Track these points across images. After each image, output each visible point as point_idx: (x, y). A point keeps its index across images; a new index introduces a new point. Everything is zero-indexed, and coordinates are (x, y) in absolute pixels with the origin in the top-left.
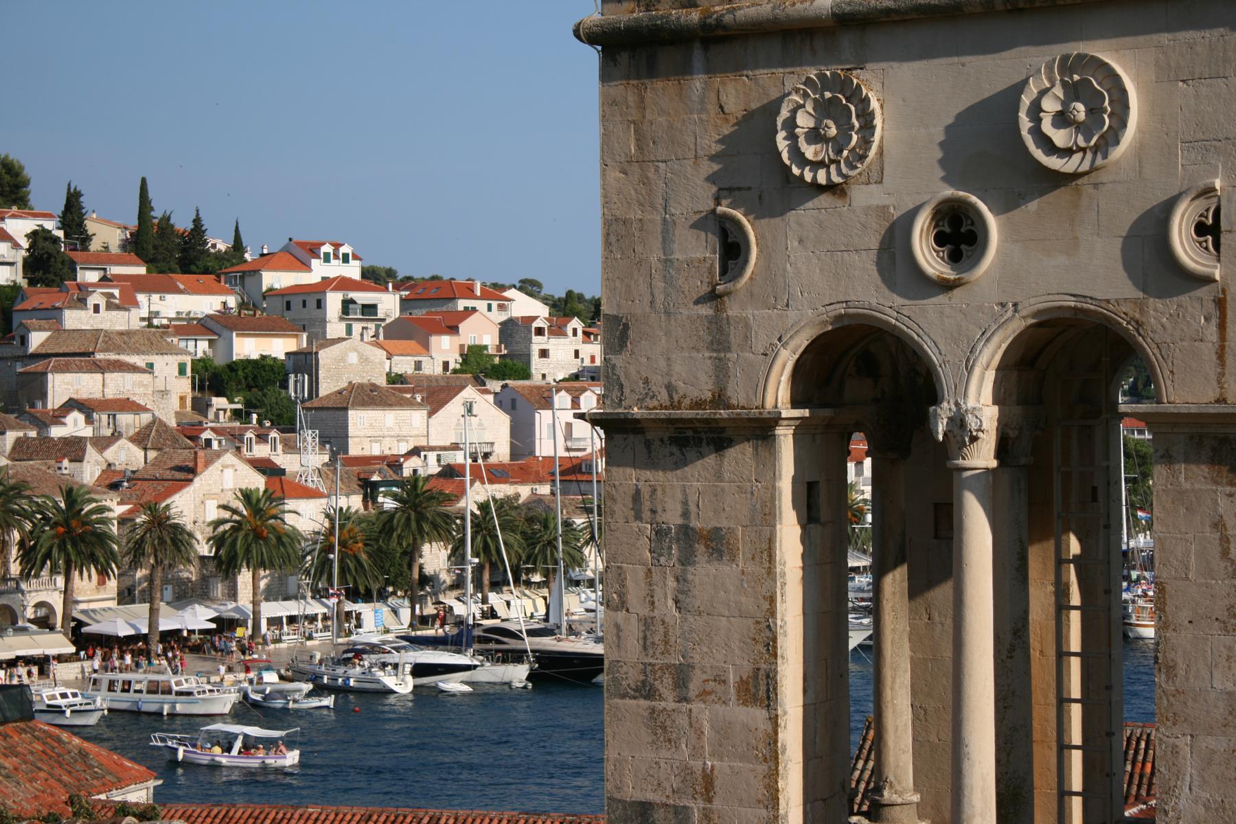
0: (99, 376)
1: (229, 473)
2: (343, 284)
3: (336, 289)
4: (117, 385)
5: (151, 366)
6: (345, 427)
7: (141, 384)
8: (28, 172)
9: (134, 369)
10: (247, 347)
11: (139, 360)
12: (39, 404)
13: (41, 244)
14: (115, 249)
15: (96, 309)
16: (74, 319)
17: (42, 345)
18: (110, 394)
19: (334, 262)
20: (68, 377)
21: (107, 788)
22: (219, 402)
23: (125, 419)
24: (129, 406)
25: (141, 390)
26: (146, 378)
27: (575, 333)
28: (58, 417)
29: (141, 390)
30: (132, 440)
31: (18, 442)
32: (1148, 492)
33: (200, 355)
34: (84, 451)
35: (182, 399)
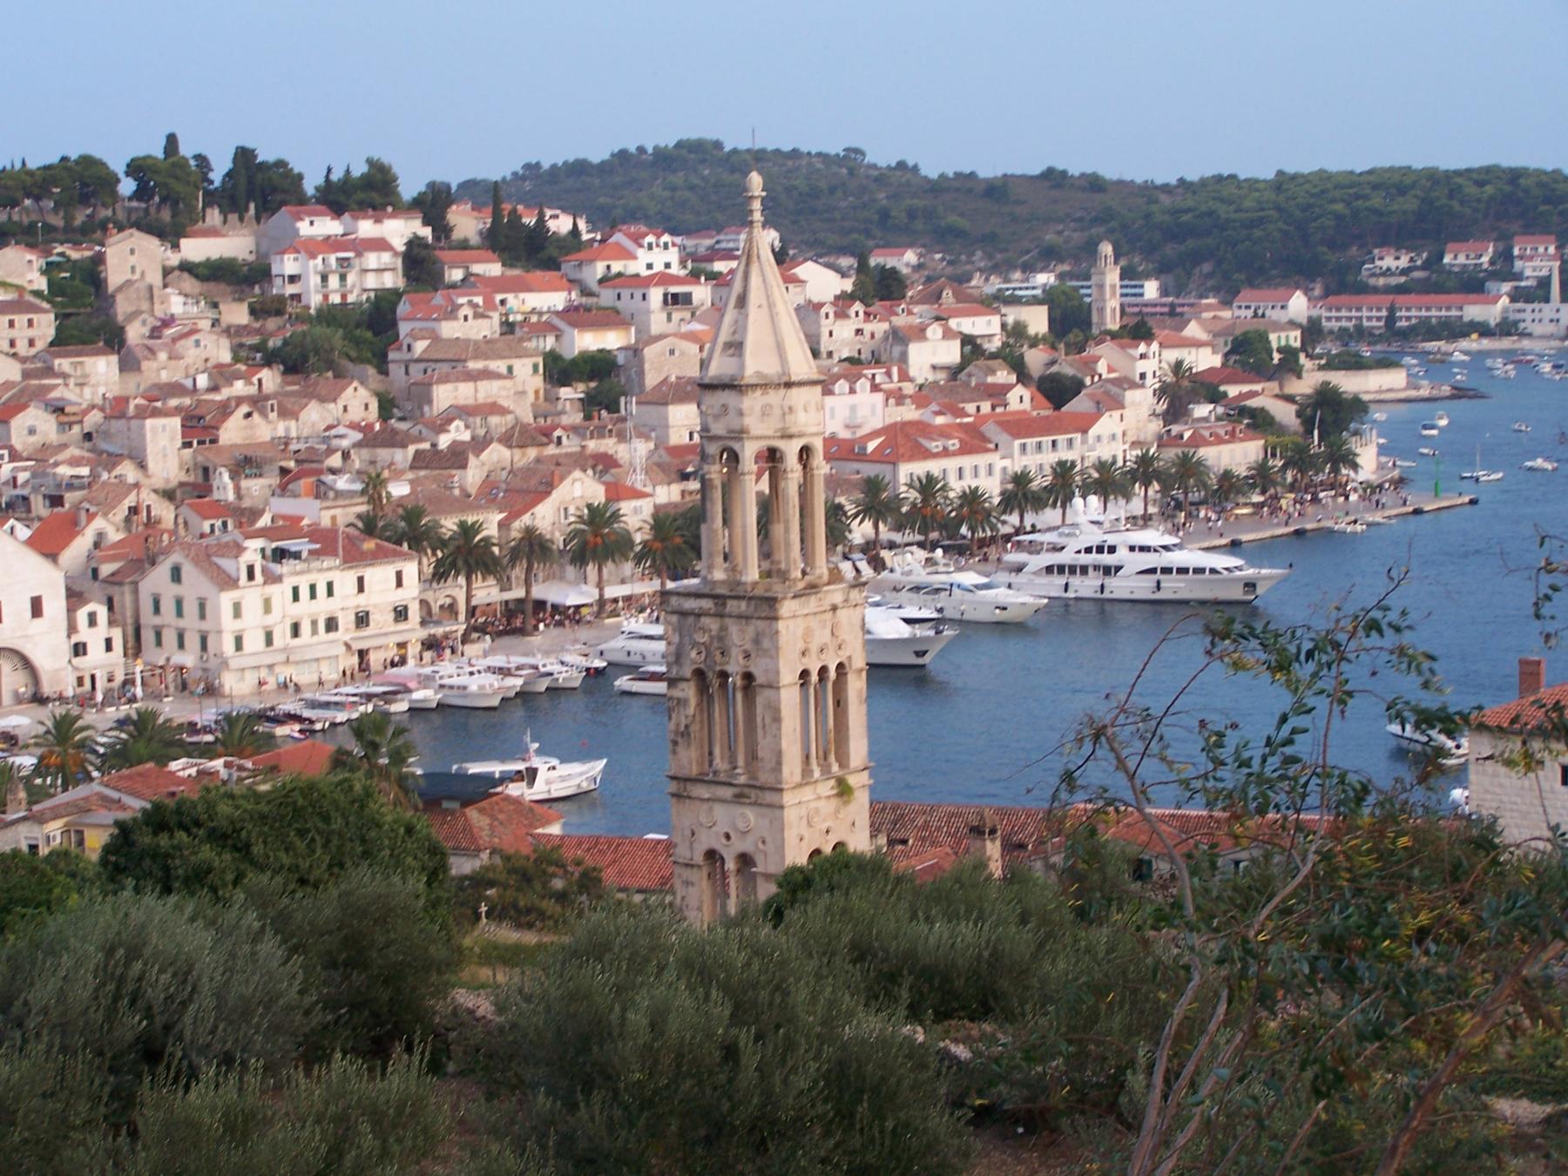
0: (471, 385)
1: (578, 485)
2: (664, 279)
3: (657, 284)
4: (487, 391)
5: (510, 369)
6: (666, 418)
7: (504, 388)
8: (396, 170)
9: (498, 376)
10: (588, 341)
11: (500, 366)
12: (426, 409)
13: (416, 251)
14: (475, 240)
15: (466, 318)
16: (449, 329)
17: (425, 351)
18: (482, 398)
19: (656, 250)
20: (449, 387)
21: (543, 825)
22: (565, 392)
23: (494, 420)
24: (495, 408)
25: (504, 393)
26: (508, 383)
27: (857, 314)
28: (442, 425)
29: (504, 393)
30: (500, 441)
31: (418, 453)
32: (523, 920)
33: (548, 348)
34: (466, 460)
35: (537, 392)
